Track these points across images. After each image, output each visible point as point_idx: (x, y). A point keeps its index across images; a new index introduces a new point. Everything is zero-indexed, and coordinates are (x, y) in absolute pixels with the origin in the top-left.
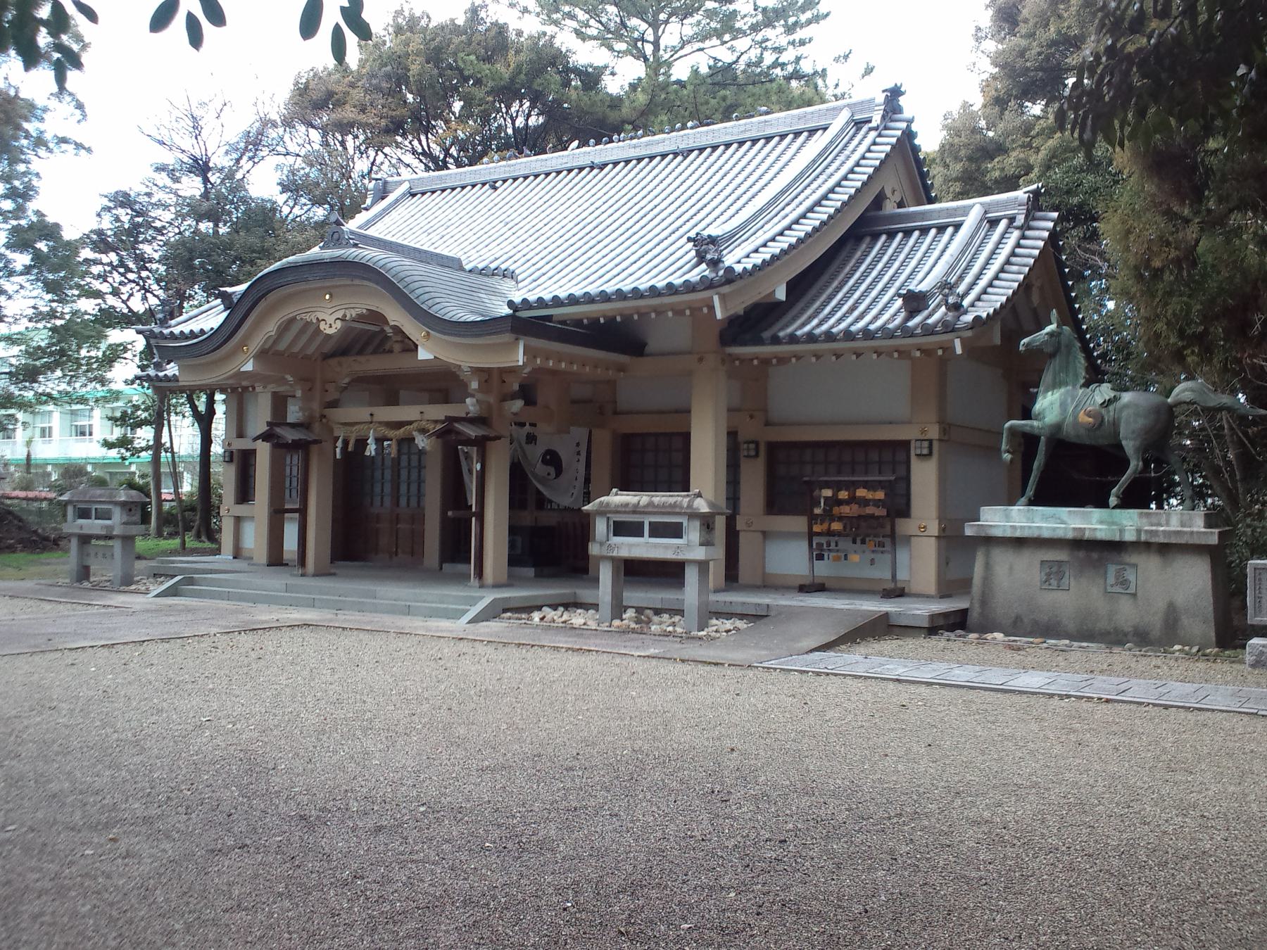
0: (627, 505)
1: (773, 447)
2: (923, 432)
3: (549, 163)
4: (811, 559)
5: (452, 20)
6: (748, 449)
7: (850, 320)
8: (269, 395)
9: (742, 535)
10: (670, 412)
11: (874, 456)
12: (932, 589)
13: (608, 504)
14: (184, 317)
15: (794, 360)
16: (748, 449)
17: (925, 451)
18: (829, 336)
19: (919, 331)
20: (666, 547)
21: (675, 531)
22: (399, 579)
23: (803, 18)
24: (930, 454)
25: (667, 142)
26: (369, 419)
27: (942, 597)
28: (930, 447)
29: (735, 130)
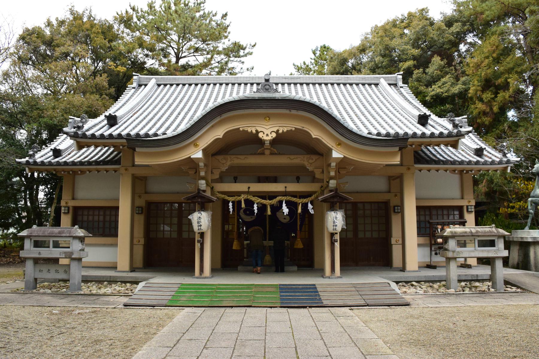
0: (466, 232)
1: (76, 209)
2: (66, 203)
3: (239, 79)
4: (431, 254)
5: (423, 11)
6: (398, 209)
7: (82, 157)
8: (130, 176)
9: (394, 246)
10: (354, 193)
11: (440, 212)
12: (127, 268)
13: (455, 233)
14: (120, 124)
15: (88, 172)
16: (398, 209)
17: (66, 211)
18: (66, 163)
19: (86, 164)
20: (488, 251)
21: (492, 244)
22: (311, 277)
23: (184, 44)
24: (68, 212)
25: (301, 79)
26: (247, 190)
27: (131, 272)
28: (69, 210)
29: (334, 79)
